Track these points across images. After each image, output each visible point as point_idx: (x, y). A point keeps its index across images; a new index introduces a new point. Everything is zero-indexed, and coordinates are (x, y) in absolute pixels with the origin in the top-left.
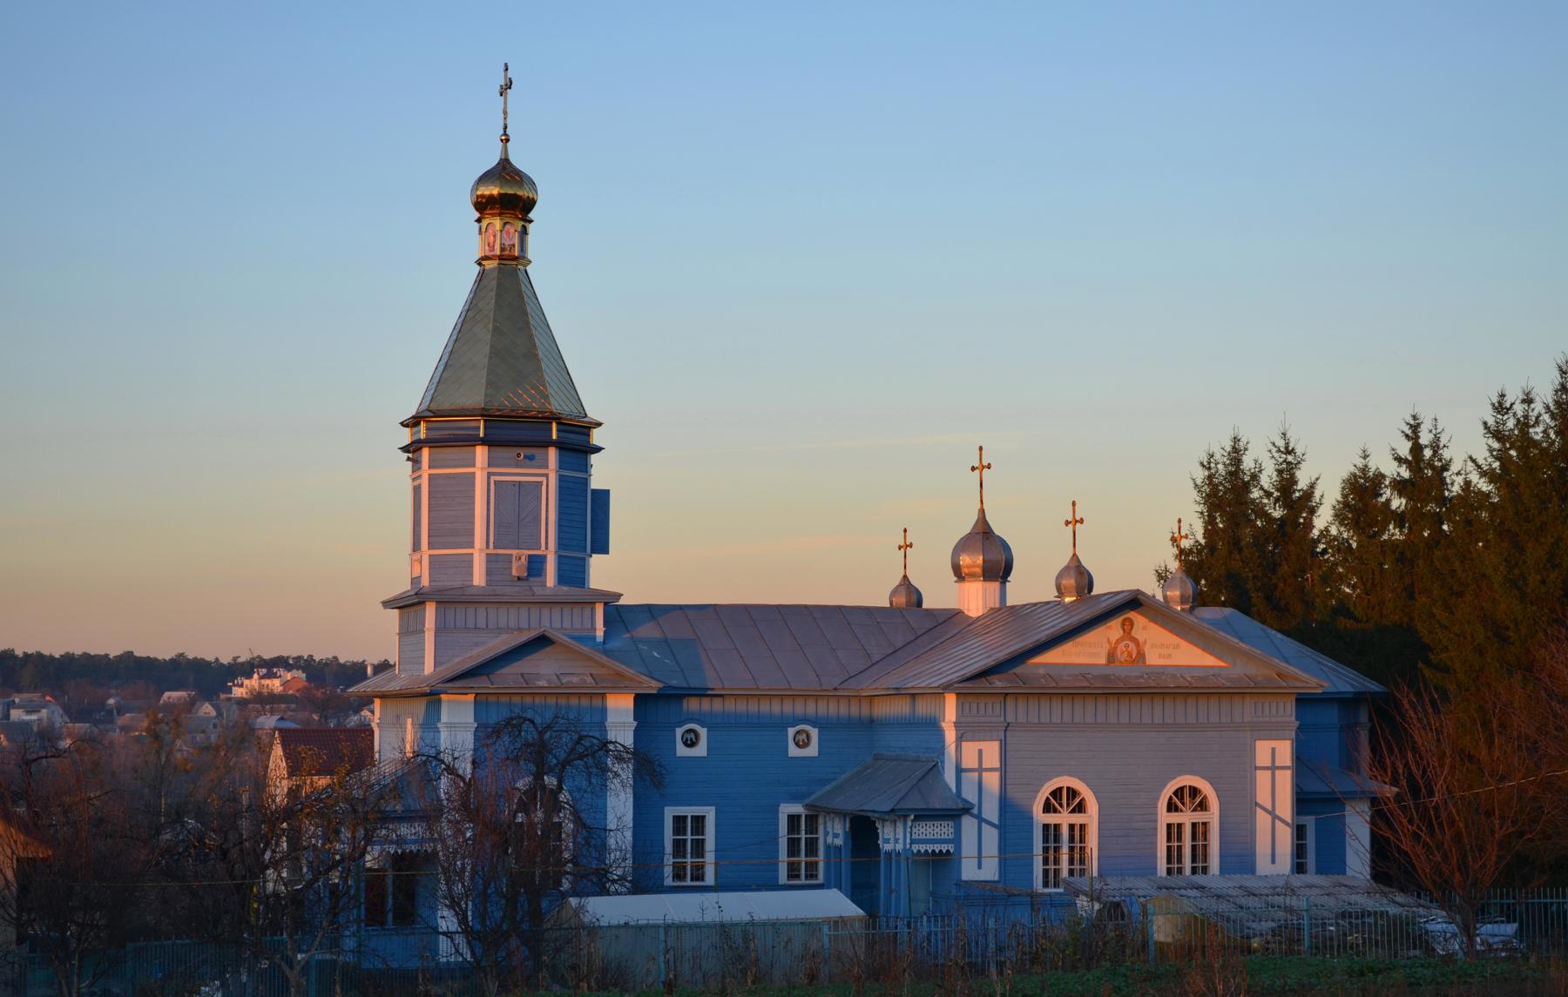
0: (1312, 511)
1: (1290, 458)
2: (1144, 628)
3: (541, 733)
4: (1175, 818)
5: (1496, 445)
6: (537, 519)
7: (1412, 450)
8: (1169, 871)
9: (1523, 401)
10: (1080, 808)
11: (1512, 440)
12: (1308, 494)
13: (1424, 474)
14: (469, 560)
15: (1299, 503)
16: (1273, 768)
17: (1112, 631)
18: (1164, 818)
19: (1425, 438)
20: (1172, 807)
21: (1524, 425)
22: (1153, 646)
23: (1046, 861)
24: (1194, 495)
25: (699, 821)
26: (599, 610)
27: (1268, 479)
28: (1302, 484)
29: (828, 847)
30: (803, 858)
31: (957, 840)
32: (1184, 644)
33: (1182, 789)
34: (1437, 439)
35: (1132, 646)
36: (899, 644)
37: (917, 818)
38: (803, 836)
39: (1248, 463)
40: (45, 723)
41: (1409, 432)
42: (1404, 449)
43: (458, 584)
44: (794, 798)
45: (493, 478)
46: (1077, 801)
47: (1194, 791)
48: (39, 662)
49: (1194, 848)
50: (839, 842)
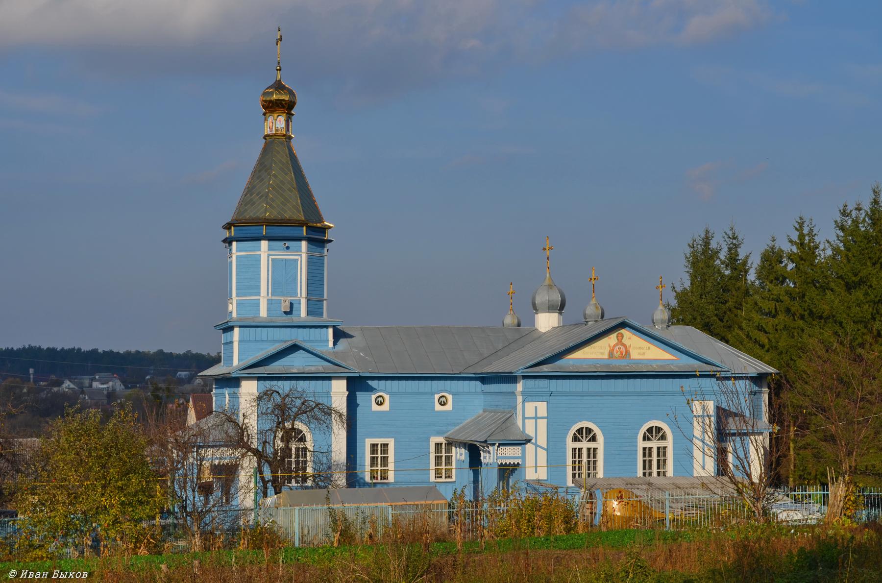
0: (746, 272)
1: (734, 241)
2: (630, 338)
3: (284, 399)
4: (648, 444)
5: (842, 234)
6: (295, 279)
7: (799, 236)
8: (644, 474)
9: (856, 209)
10: (593, 439)
11: (850, 232)
12: (745, 263)
13: (806, 249)
14: (257, 304)
15: (738, 267)
16: (536, 418)
17: (612, 339)
18: (641, 444)
19: (806, 231)
20: (646, 438)
21: (855, 222)
22: (635, 348)
23: (574, 468)
24: (684, 262)
25: (385, 446)
26: (331, 331)
27: (723, 255)
28: (741, 257)
29: (457, 460)
30: (443, 467)
31: (523, 457)
32: (652, 347)
33: (652, 428)
34: (811, 231)
35: (623, 348)
36: (500, 347)
37: (500, 445)
38: (444, 454)
39: (713, 245)
40: (110, 389)
41: (797, 227)
42: (795, 236)
43: (251, 316)
44: (439, 433)
45: (271, 257)
46: (660, 434)
47: (659, 429)
48: (110, 355)
49: (658, 461)
50: (463, 458)
